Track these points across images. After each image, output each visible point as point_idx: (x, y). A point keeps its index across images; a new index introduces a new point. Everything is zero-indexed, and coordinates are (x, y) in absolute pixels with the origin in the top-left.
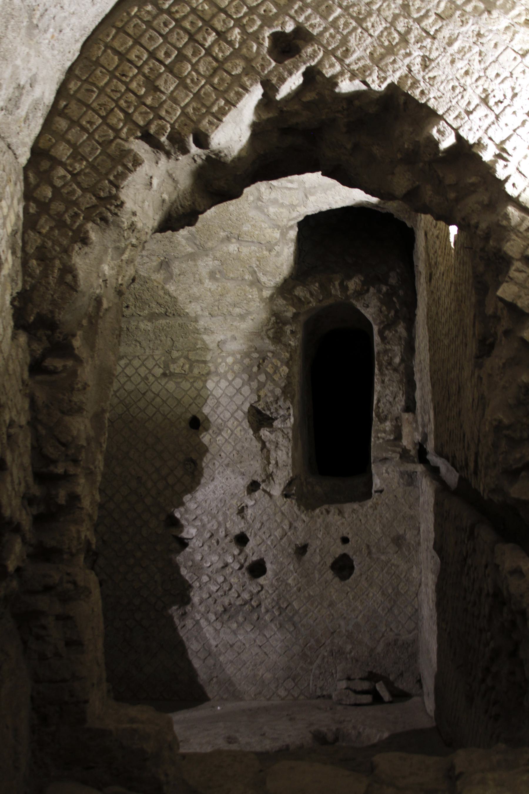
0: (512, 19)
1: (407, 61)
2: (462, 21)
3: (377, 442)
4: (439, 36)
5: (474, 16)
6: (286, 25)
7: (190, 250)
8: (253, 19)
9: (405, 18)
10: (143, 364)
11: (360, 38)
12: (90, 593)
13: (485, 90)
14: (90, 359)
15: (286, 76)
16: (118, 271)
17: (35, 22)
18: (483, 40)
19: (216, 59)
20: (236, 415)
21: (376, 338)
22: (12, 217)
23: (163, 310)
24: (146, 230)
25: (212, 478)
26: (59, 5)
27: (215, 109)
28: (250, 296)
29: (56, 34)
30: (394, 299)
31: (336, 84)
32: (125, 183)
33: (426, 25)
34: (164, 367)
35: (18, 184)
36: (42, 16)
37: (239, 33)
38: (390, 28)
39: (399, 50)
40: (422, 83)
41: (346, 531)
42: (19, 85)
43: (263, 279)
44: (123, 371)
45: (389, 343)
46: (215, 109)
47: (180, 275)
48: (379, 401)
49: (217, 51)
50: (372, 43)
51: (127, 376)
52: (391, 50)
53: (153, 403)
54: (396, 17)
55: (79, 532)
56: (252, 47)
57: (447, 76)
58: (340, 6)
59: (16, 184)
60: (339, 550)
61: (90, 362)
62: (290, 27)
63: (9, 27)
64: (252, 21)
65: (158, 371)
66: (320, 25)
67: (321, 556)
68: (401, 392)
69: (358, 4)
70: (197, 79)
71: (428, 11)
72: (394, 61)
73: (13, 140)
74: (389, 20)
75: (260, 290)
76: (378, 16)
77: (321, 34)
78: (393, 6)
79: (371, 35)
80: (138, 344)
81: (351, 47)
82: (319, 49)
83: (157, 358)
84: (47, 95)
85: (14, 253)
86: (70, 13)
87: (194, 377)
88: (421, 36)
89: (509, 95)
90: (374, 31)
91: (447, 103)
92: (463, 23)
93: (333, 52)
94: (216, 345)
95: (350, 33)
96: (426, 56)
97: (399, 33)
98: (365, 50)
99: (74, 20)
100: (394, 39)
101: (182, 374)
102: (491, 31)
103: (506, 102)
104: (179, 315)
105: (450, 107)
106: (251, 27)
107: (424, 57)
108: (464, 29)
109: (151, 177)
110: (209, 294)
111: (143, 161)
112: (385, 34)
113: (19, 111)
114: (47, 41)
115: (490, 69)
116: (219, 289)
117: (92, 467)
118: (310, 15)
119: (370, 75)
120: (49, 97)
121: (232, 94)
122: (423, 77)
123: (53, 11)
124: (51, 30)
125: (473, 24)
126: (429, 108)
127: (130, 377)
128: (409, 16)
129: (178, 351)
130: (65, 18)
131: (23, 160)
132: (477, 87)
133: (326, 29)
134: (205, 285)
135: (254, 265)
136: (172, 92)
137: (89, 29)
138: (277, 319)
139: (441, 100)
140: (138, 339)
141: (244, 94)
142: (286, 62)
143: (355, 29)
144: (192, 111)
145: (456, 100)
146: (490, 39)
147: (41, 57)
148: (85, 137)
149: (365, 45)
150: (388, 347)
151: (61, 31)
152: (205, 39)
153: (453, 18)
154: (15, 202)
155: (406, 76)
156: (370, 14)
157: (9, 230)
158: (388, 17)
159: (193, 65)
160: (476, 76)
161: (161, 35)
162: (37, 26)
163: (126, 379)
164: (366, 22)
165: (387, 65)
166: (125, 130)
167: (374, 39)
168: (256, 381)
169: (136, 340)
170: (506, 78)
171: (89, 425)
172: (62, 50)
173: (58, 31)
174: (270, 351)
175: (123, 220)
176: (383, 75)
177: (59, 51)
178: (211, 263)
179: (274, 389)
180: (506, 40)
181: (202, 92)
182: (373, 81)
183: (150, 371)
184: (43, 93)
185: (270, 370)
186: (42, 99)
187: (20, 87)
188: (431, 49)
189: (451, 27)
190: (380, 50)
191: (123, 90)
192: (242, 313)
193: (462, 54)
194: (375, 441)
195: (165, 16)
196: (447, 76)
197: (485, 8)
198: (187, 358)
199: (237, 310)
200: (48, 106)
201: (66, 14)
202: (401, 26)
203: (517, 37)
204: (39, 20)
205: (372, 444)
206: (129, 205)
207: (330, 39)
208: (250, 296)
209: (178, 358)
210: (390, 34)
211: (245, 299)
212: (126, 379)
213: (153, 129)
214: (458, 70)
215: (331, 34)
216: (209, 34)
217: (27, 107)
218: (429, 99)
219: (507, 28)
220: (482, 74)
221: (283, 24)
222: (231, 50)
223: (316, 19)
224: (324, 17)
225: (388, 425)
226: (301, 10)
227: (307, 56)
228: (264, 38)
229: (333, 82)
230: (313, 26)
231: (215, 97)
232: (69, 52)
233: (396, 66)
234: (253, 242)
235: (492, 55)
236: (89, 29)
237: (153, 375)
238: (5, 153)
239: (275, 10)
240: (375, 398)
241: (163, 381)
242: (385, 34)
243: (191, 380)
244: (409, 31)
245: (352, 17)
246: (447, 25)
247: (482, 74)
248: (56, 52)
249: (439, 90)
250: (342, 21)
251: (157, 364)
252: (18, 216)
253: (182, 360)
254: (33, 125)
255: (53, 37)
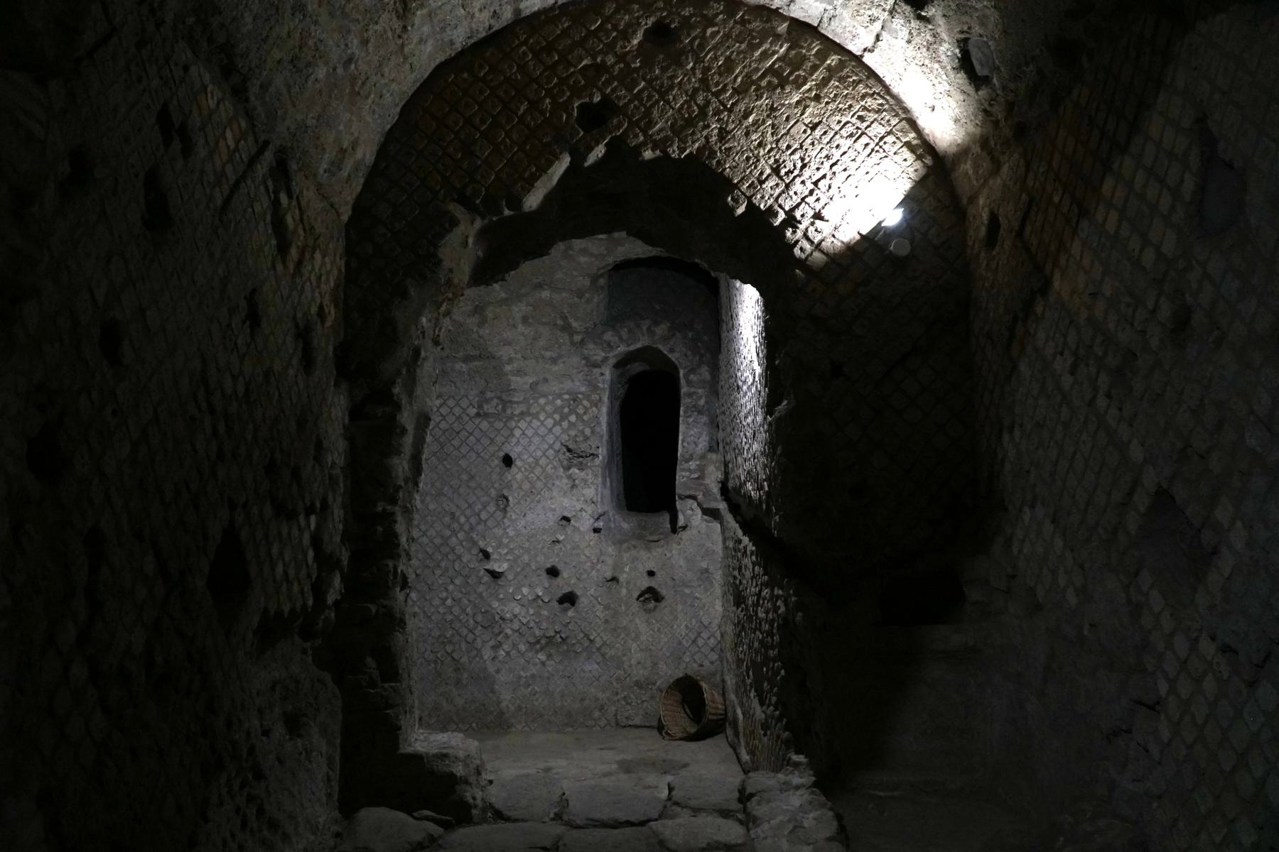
0: (803, 94)
1: (705, 133)
2: (757, 95)
3: (682, 480)
4: (737, 109)
5: (768, 91)
6: (594, 95)
7: (503, 295)
8: (564, 90)
9: (704, 91)
10: (458, 404)
11: (662, 111)
12: (405, 624)
13: (776, 161)
14: (408, 405)
15: (593, 145)
16: (435, 324)
17: (357, 89)
18: (778, 114)
19: (528, 127)
20: (547, 454)
21: (683, 382)
22: (335, 272)
23: (477, 353)
24: (462, 285)
25: (523, 514)
26: (379, 74)
27: (527, 174)
28: (562, 341)
29: (377, 100)
30: (699, 344)
31: (640, 154)
32: (443, 242)
33: (723, 98)
34: (478, 407)
35: (341, 240)
36: (363, 84)
37: (549, 103)
38: (690, 101)
39: (698, 122)
40: (719, 154)
41: (651, 565)
42: (342, 149)
43: (575, 324)
44: (438, 411)
45: (693, 386)
46: (527, 174)
47: (494, 319)
48: (683, 441)
49: (529, 119)
50: (673, 115)
51: (441, 415)
52: (690, 122)
53: (467, 442)
54: (696, 91)
55: (395, 568)
56: (562, 116)
57: (742, 148)
58: (644, 79)
59: (338, 240)
60: (645, 583)
61: (408, 408)
62: (597, 99)
63: (333, 96)
64: (563, 92)
65: (473, 411)
66: (625, 97)
67: (627, 589)
68: (705, 433)
69: (661, 78)
70: (511, 145)
71: (725, 86)
72: (693, 134)
73: (335, 200)
74: (690, 93)
75: (571, 335)
76: (679, 89)
77: (626, 105)
78: (693, 80)
79: (671, 107)
80: (453, 385)
81: (654, 119)
82: (624, 120)
83: (471, 398)
84: (368, 156)
85: (336, 306)
86: (390, 80)
87: (507, 417)
88: (719, 109)
89: (799, 165)
90: (675, 104)
91: (741, 173)
92: (759, 97)
93: (637, 123)
94: (528, 386)
95: (652, 106)
96: (723, 128)
97: (698, 105)
98: (667, 122)
99: (394, 86)
100: (694, 111)
101: (495, 413)
102: (783, 105)
103: (796, 172)
104: (494, 358)
105: (744, 177)
106: (561, 98)
107: (720, 129)
108: (758, 103)
109: (467, 237)
110: (522, 338)
111: (460, 222)
112: (686, 106)
113: (342, 172)
114: (368, 106)
115: (781, 141)
116: (532, 333)
117: (408, 505)
118: (616, 87)
119: (671, 145)
120: (370, 158)
121: (543, 161)
122: (720, 148)
123: (374, 79)
124: (372, 96)
125: (766, 99)
126: (725, 176)
127: (445, 417)
128: (708, 89)
129: (491, 392)
130: (386, 84)
131: (345, 218)
132: (769, 158)
133: (630, 101)
134: (519, 330)
135: (566, 311)
136: (487, 157)
137: (408, 95)
138: (587, 362)
139: (736, 170)
140: (452, 380)
141: (555, 162)
142: (594, 132)
143: (657, 102)
144: (505, 176)
145: (749, 170)
146: (783, 113)
147: (362, 121)
148: (404, 198)
149: (666, 116)
150: (693, 390)
151: (381, 97)
152: (518, 108)
153: (749, 92)
154: (338, 259)
155: (704, 146)
156: (671, 88)
157: (332, 284)
158: (688, 90)
159: (506, 133)
160: (769, 147)
161: (477, 102)
162: (359, 93)
163: (441, 418)
164: (668, 96)
165: (686, 136)
166: (442, 192)
167: (675, 111)
168: (567, 422)
169: (451, 381)
170: (796, 150)
171: (406, 467)
172: (382, 114)
173: (378, 96)
174: (580, 393)
175: (441, 276)
176: (682, 146)
177: (380, 115)
178: (524, 308)
179: (584, 429)
180: (797, 113)
181: (515, 158)
182: (674, 151)
183: (464, 410)
184: (364, 155)
185: (581, 411)
186: (364, 160)
187: (342, 151)
188: (728, 121)
189: (746, 101)
190: (680, 122)
191: (440, 154)
192: (554, 356)
193: (756, 126)
194: (679, 479)
195: (481, 84)
196: (742, 147)
197: (779, 83)
198: (499, 398)
199: (548, 354)
200: (369, 167)
201: (387, 81)
202: (700, 100)
203: (809, 111)
204: (361, 88)
205: (677, 482)
206: (446, 264)
207: (635, 111)
208: (562, 341)
209: (492, 399)
210: (689, 107)
211: (557, 343)
212: (441, 418)
213: (469, 192)
214: (752, 141)
215: (635, 106)
216: (522, 103)
217: (349, 168)
218: (726, 169)
219: (798, 103)
220: (774, 146)
221: (591, 96)
222: (542, 118)
223: (621, 91)
224: (630, 90)
225: (693, 465)
226: (608, 82)
227: (612, 126)
228: (573, 107)
229: (638, 150)
230: (619, 98)
231: (526, 163)
232: (389, 116)
233: (695, 137)
234: (564, 289)
235: (783, 128)
236: (408, 95)
237: (468, 415)
238: (328, 212)
239: (583, 82)
240: (680, 438)
241: (477, 421)
242: (686, 106)
243: (504, 420)
244: (708, 103)
245: (656, 90)
246: (743, 99)
247: (774, 146)
248: (377, 116)
249: (734, 161)
250: (646, 94)
251: (471, 404)
252: (340, 271)
253: (496, 401)
254: (354, 185)
255: (373, 102)
